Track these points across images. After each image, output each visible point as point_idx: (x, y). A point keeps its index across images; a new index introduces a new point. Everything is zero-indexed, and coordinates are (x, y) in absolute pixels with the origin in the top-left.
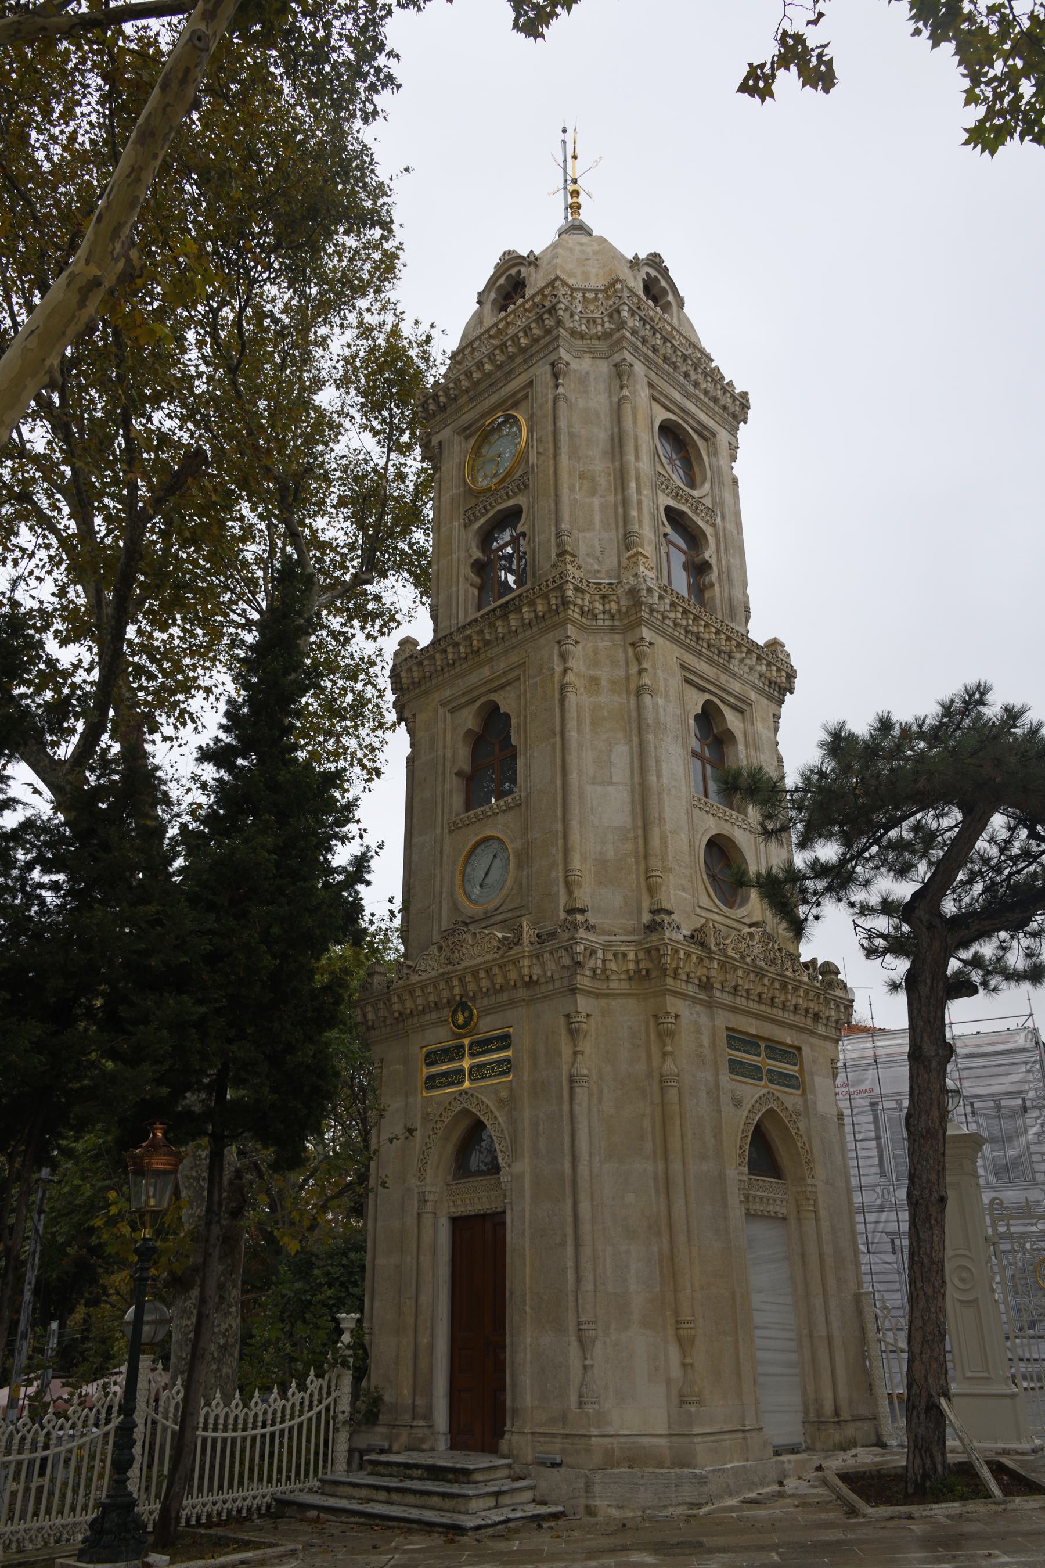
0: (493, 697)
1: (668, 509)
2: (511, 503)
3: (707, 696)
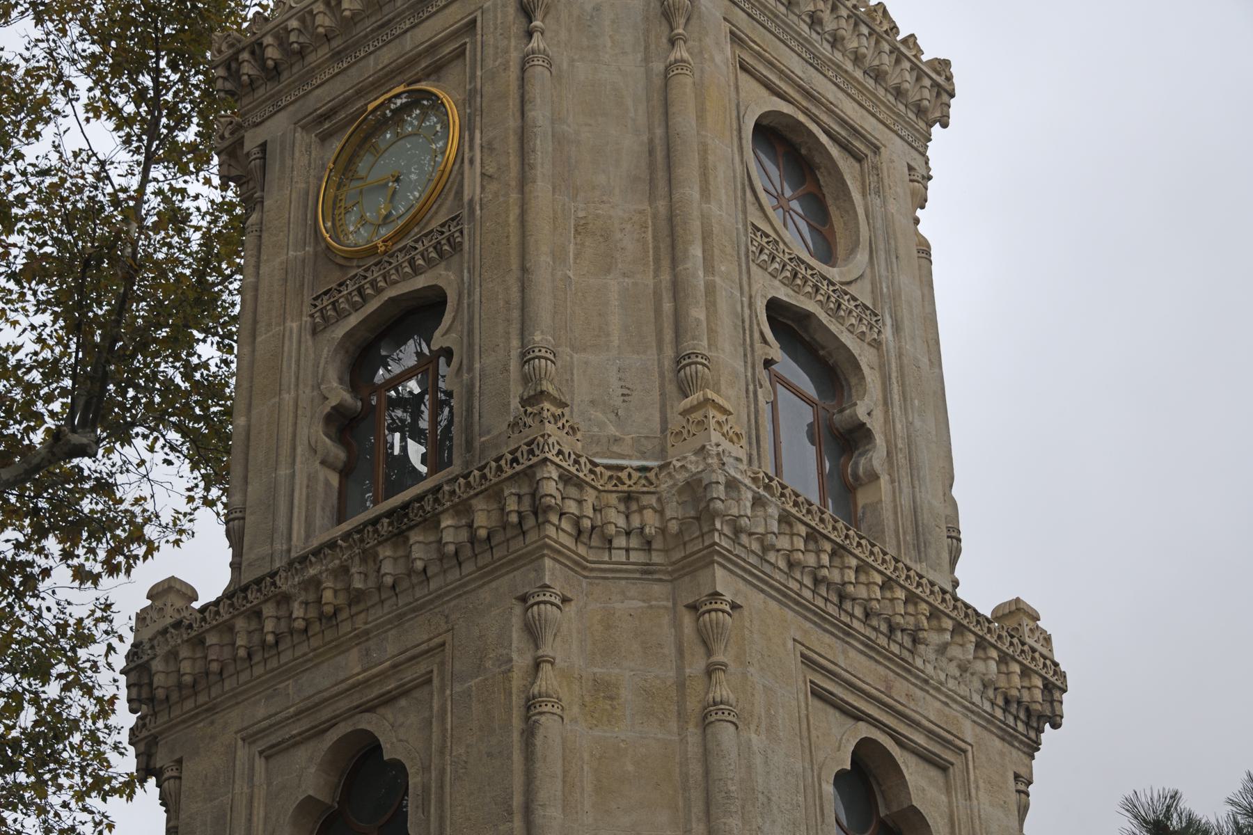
0: (366, 722)
1: (775, 307)
2: (420, 282)
3: (865, 731)
